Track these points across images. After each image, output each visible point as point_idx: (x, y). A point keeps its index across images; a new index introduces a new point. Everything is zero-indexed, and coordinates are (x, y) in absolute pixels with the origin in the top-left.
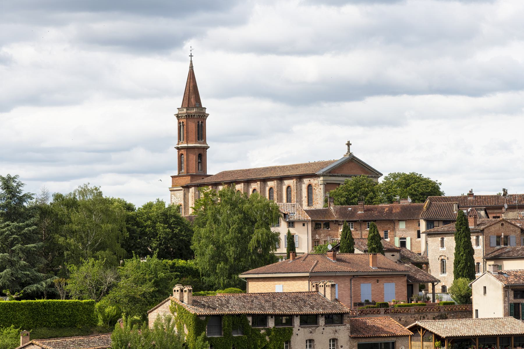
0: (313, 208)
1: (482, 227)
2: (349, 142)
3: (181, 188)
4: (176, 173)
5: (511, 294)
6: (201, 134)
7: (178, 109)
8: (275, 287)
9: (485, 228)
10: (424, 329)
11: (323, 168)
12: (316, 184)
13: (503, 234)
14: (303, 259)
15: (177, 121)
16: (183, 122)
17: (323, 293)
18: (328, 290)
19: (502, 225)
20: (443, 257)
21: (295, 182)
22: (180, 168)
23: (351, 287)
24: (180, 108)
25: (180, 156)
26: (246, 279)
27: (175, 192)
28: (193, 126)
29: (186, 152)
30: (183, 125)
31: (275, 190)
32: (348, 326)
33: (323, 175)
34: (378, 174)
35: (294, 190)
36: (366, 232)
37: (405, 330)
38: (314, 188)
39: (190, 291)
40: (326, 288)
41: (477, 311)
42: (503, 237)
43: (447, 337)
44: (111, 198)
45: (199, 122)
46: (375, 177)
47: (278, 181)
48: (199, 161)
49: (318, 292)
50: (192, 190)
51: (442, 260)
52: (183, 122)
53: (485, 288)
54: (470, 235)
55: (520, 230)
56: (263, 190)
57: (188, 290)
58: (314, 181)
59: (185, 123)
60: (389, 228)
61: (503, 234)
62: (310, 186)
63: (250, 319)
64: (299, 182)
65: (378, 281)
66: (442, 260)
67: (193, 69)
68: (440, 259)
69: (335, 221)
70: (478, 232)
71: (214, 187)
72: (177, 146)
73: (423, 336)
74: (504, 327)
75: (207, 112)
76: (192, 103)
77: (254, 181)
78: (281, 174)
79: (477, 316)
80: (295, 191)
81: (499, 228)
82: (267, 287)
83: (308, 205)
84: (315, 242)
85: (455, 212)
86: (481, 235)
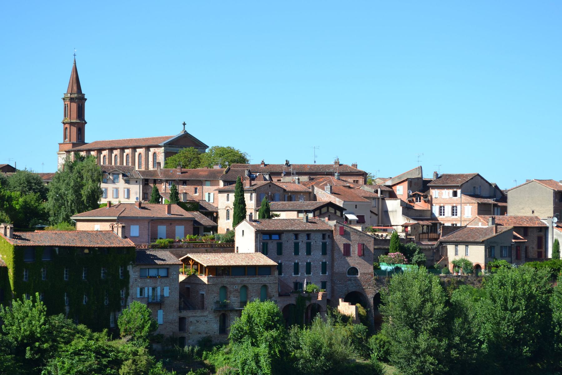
0: (140, 170)
3: (65, 152)
4: (62, 142)
7: (64, 94)
8: (94, 226)
10: (193, 260)
11: (165, 141)
12: (159, 152)
13: (270, 193)
14: (116, 206)
15: (63, 103)
16: (67, 104)
17: (116, 232)
18: (120, 230)
19: (270, 186)
20: (228, 208)
21: (144, 150)
22: (65, 138)
23: (149, 228)
25: (66, 129)
26: (76, 220)
27: (61, 155)
28: (74, 106)
30: (67, 106)
36: (169, 187)
37: (179, 261)
39: (11, 228)
40: (119, 228)
41: (237, 247)
43: (207, 266)
44: (237, 149)
45: (79, 105)
46: (203, 149)
47: (121, 150)
49: (113, 231)
51: (227, 210)
52: (67, 104)
53: (243, 231)
54: (244, 193)
55: (283, 190)
56: (98, 158)
57: (10, 227)
58: (157, 150)
61: (270, 193)
62: (154, 154)
63: (57, 249)
65: (171, 224)
66: (227, 210)
68: (226, 209)
70: (252, 191)
73: (192, 265)
74: (252, 260)
75: (85, 97)
76: (74, 90)
78: (135, 144)
79: (237, 252)
81: (267, 188)
82: (89, 226)
83: (139, 168)
84: (145, 194)
85: (246, 176)
86: (254, 193)
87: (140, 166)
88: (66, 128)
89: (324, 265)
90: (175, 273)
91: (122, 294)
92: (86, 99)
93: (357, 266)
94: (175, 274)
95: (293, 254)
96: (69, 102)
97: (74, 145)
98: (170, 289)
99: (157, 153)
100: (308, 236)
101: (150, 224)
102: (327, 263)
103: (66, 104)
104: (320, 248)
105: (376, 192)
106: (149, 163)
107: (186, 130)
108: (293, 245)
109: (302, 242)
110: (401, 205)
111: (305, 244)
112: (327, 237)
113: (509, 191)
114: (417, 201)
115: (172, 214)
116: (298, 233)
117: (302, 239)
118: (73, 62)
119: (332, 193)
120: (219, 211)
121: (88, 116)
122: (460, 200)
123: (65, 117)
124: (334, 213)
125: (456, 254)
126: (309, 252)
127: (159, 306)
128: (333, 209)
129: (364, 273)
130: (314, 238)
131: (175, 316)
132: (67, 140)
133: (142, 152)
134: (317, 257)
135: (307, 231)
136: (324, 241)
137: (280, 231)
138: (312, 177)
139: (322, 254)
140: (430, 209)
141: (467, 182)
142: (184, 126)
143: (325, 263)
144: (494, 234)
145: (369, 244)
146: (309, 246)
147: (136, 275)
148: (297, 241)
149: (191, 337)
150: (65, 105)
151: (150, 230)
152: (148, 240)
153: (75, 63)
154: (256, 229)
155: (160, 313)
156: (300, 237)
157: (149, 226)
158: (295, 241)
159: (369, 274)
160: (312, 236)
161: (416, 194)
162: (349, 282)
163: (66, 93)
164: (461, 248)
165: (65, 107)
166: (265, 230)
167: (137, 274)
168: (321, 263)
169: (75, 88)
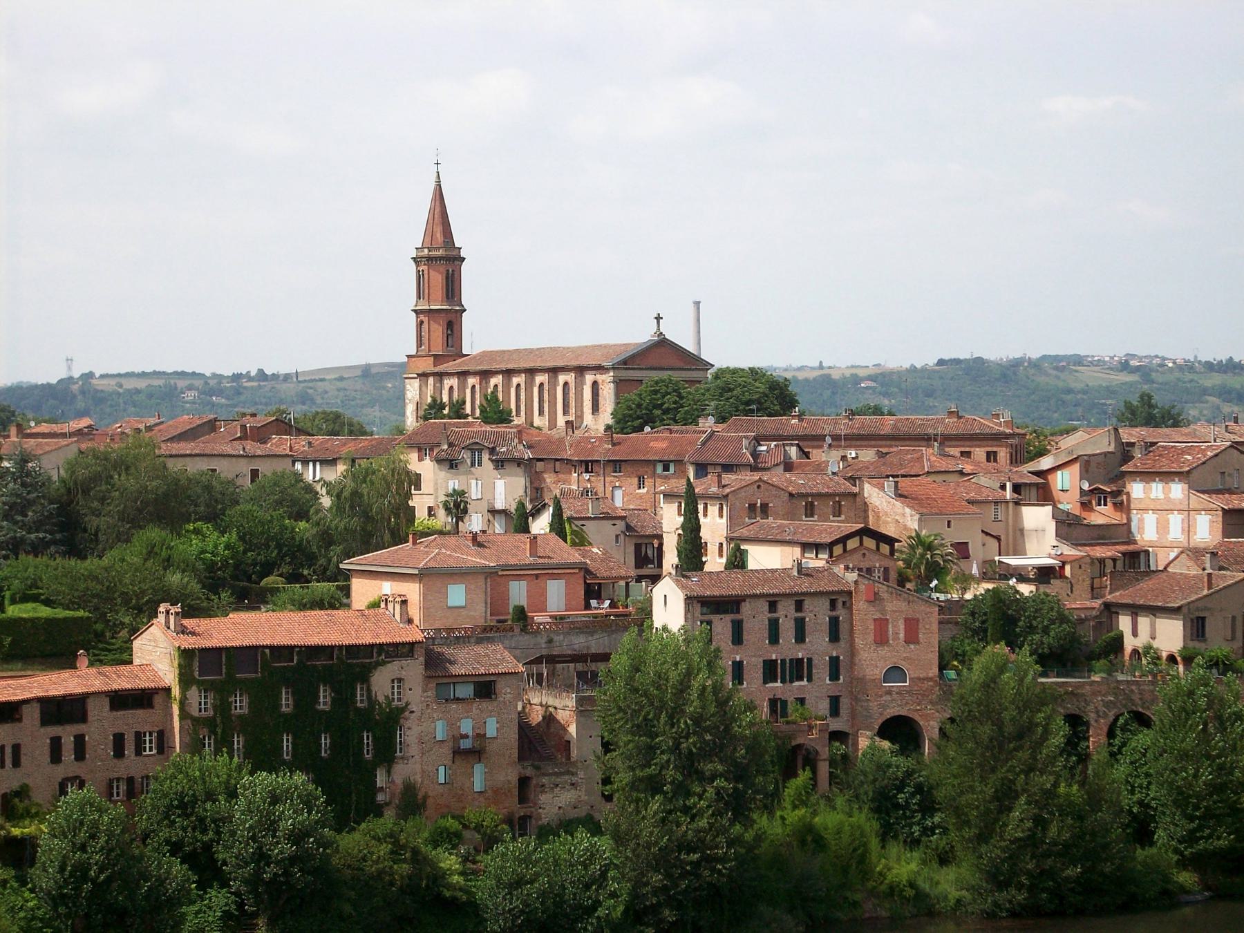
1: (727, 490)
5: (698, 607)
6: (452, 288)
9: (732, 492)
13: (759, 501)
16: (423, 271)
19: (759, 487)
22: (420, 343)
26: (349, 570)
28: (437, 279)
30: (423, 275)
32: (422, 659)
33: (614, 368)
42: (759, 505)
45: (448, 271)
48: (449, 332)
50: (431, 380)
52: (423, 271)
53: (665, 596)
55: (787, 495)
58: (600, 378)
59: (426, 272)
61: (759, 501)
62: (595, 383)
63: (267, 651)
69: (567, 459)
76: (437, 238)
77: (516, 372)
87: (566, 409)
88: (422, 322)
89: (834, 663)
90: (508, 691)
91: (368, 743)
92: (464, 259)
93: (904, 663)
94: (510, 693)
95: (767, 642)
96: (426, 267)
98: (498, 722)
99: (600, 382)
100: (799, 606)
101: (489, 580)
102: (841, 658)
104: (826, 628)
105: (1003, 487)
106: (585, 404)
107: (661, 331)
108: (767, 623)
109: (786, 616)
110: (1053, 518)
111: (793, 622)
112: (840, 605)
114: (1100, 505)
115: (539, 557)
116: (777, 599)
117: (786, 613)
118: (436, 174)
119: (901, 496)
120: (665, 535)
121: (468, 295)
122: (1187, 503)
124: (874, 547)
125: (1135, 633)
126: (800, 637)
127: (477, 757)
128: (874, 542)
129: (919, 679)
130: (811, 608)
131: (509, 775)
133: (569, 381)
134: (818, 646)
135: (796, 594)
136: (834, 613)
137: (737, 596)
138: (884, 450)
139: (830, 640)
140: (1125, 521)
141: (1204, 463)
142: (658, 323)
143: (838, 658)
144: (1205, 592)
145: (928, 617)
146: (800, 627)
147: (428, 697)
148: (774, 615)
149: (543, 816)
150: (419, 271)
151: (489, 594)
152: (486, 612)
154: (686, 595)
155: (479, 770)
156: (780, 606)
157: (486, 584)
158: (769, 615)
159: (930, 679)
160: (808, 604)
161: (1095, 489)
162: (888, 698)
163: (420, 246)
164: (1144, 622)
166: (704, 597)
167: (429, 693)
168: (827, 658)
169: (439, 236)
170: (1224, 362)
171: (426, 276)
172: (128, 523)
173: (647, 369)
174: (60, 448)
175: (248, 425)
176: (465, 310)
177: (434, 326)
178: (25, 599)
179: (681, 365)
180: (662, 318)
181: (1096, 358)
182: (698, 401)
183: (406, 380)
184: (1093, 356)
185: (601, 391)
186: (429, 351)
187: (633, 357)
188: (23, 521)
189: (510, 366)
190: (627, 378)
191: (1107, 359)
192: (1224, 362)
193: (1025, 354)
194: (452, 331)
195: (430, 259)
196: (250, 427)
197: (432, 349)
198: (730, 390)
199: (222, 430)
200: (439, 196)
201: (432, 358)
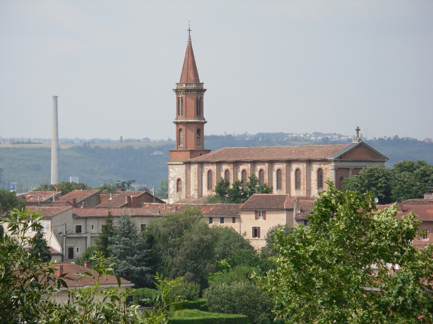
2: (358, 127)
16: (182, 98)
24: (179, 84)
25: (179, 131)
28: (191, 103)
29: (185, 127)
30: (182, 100)
31: (284, 172)
34: (384, 158)
35: (304, 173)
38: (325, 172)
45: (197, 98)
47: (287, 164)
48: (198, 136)
52: (182, 98)
59: (184, 99)
60: (429, 229)
64: (309, 166)
67: (191, 44)
71: (218, 165)
72: (176, 121)
80: (305, 175)
97: (193, 153)
103: (180, 97)
106: (312, 183)
113: (31, 204)
118: (187, 39)
123: (179, 115)
132: (181, 145)
142: (358, 133)
150: (179, 98)
153: (190, 39)
165: (179, 101)
169: (192, 76)
170: (392, 139)
171: (184, 101)
172: (192, 260)
173: (352, 161)
174: (63, 212)
175: (131, 196)
176: (206, 122)
177: (189, 132)
178: (185, 306)
179: (370, 159)
180: (360, 130)
181: (294, 135)
182: (407, 182)
183: (169, 166)
184: (292, 134)
185: (324, 175)
186: (186, 148)
187: (345, 154)
188: (130, 260)
189: (255, 158)
190: (341, 167)
191: (302, 136)
192: (392, 139)
193: (247, 132)
194: (199, 135)
195: (187, 90)
196: (133, 197)
197: (188, 146)
198: (428, 176)
199: (111, 199)
200: (190, 51)
201: (189, 153)
